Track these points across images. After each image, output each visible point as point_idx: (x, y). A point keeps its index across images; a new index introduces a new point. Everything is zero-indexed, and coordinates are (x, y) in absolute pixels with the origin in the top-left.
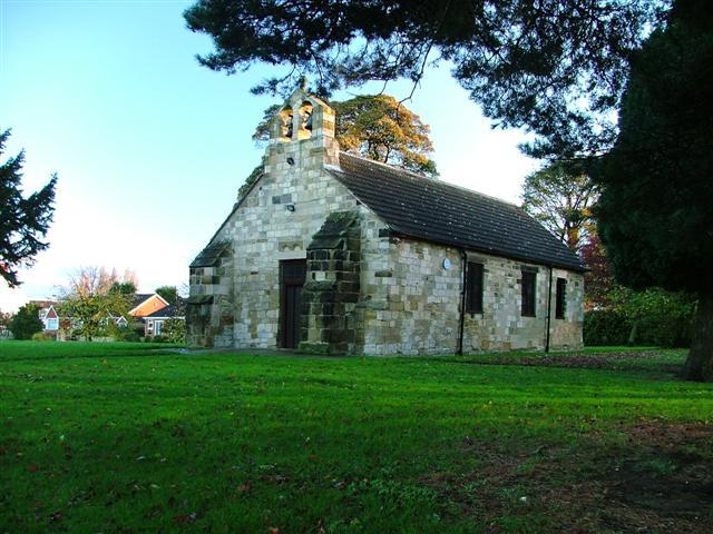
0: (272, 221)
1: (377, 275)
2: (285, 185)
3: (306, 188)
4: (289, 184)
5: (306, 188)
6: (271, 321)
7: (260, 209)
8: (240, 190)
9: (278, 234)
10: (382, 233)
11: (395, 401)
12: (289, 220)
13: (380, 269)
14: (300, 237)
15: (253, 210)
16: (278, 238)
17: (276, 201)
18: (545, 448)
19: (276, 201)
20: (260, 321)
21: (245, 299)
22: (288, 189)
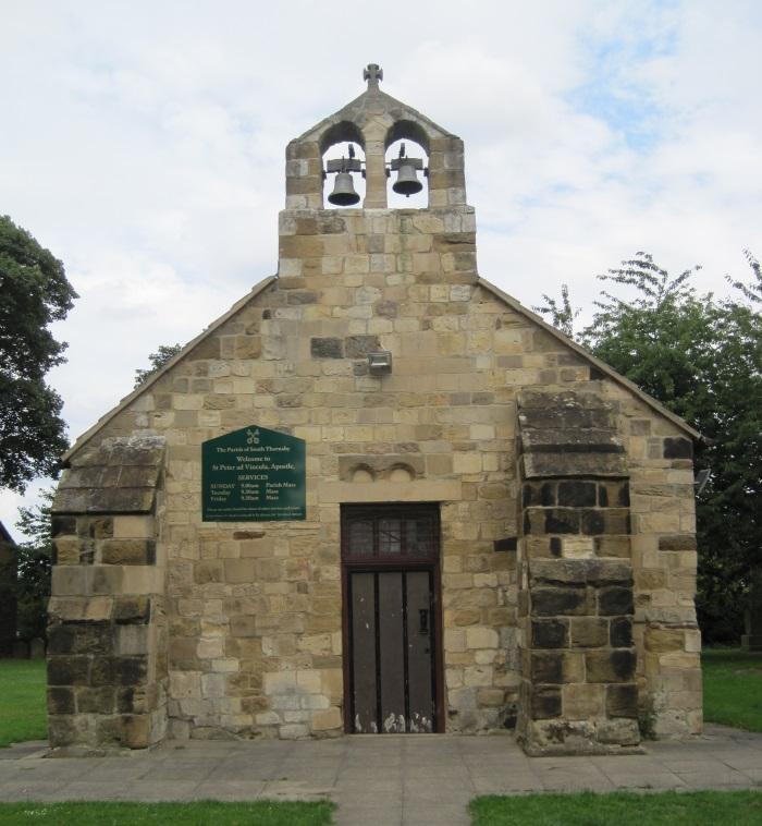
0: (309, 399)
1: (665, 545)
2: (354, 311)
3: (427, 325)
4: (369, 311)
5: (427, 325)
6: (319, 663)
7: (264, 369)
8: (59, 263)
9: (339, 435)
10: (673, 450)
11: (30, 756)
12: (372, 401)
13: (673, 531)
14: (416, 448)
15: (241, 367)
16: (338, 448)
17: (324, 349)
18: (578, 805)
19: (324, 349)
20: (271, 664)
21: (213, 606)
22: (360, 321)
